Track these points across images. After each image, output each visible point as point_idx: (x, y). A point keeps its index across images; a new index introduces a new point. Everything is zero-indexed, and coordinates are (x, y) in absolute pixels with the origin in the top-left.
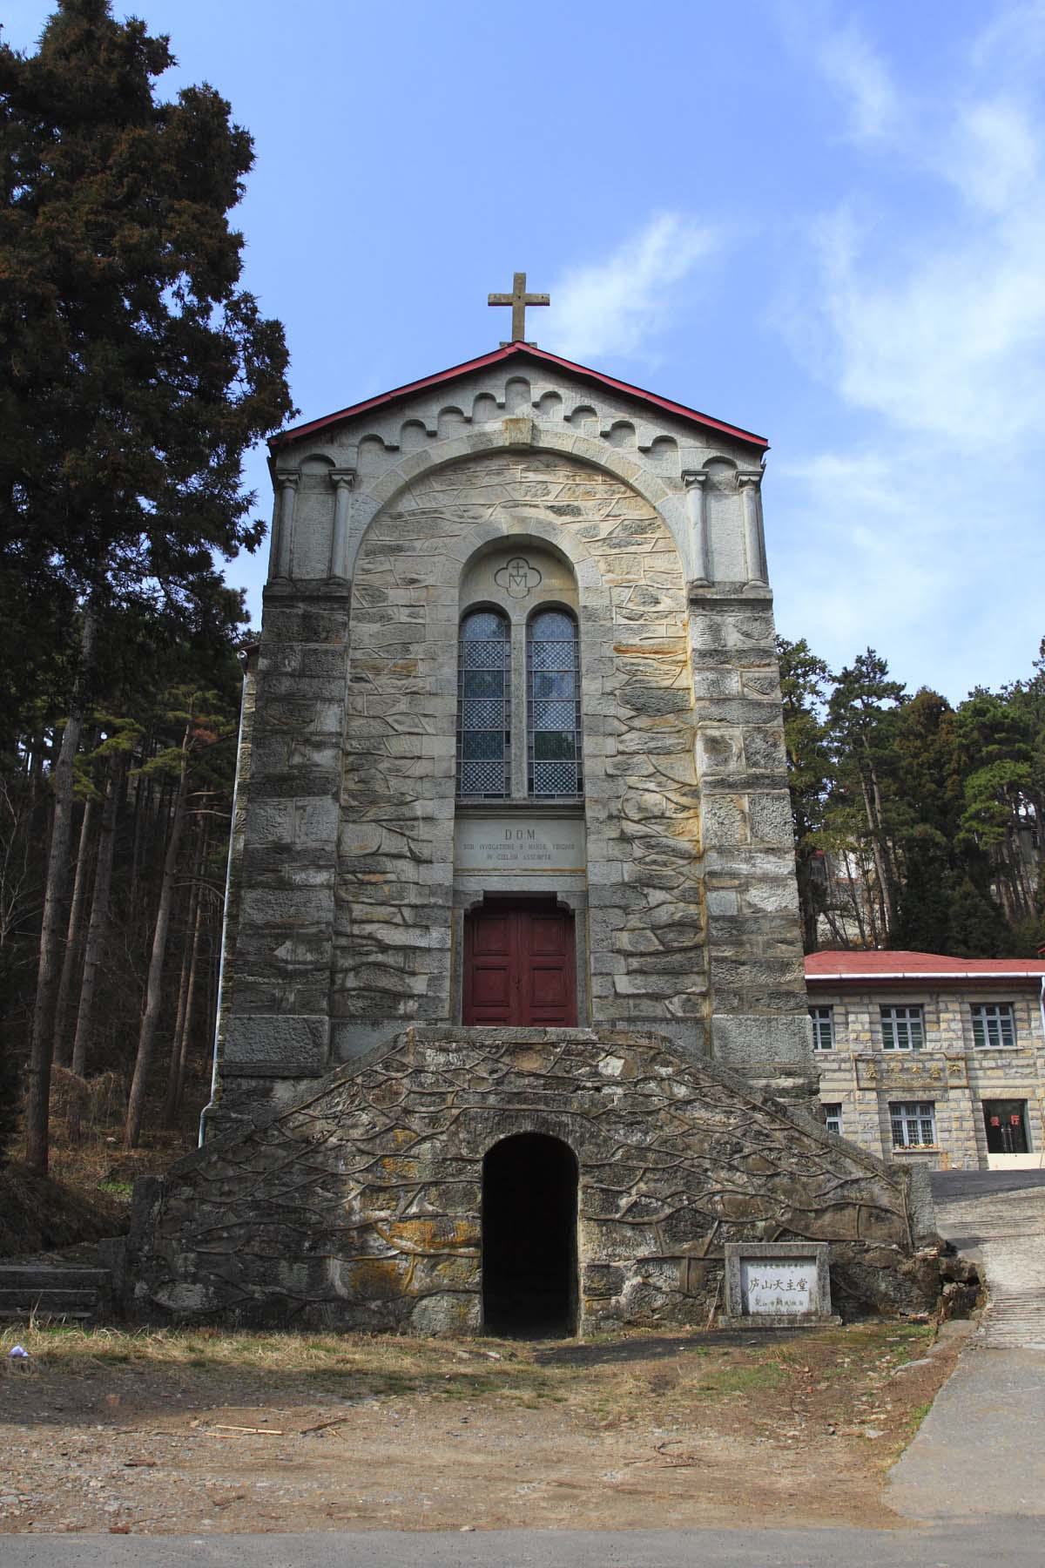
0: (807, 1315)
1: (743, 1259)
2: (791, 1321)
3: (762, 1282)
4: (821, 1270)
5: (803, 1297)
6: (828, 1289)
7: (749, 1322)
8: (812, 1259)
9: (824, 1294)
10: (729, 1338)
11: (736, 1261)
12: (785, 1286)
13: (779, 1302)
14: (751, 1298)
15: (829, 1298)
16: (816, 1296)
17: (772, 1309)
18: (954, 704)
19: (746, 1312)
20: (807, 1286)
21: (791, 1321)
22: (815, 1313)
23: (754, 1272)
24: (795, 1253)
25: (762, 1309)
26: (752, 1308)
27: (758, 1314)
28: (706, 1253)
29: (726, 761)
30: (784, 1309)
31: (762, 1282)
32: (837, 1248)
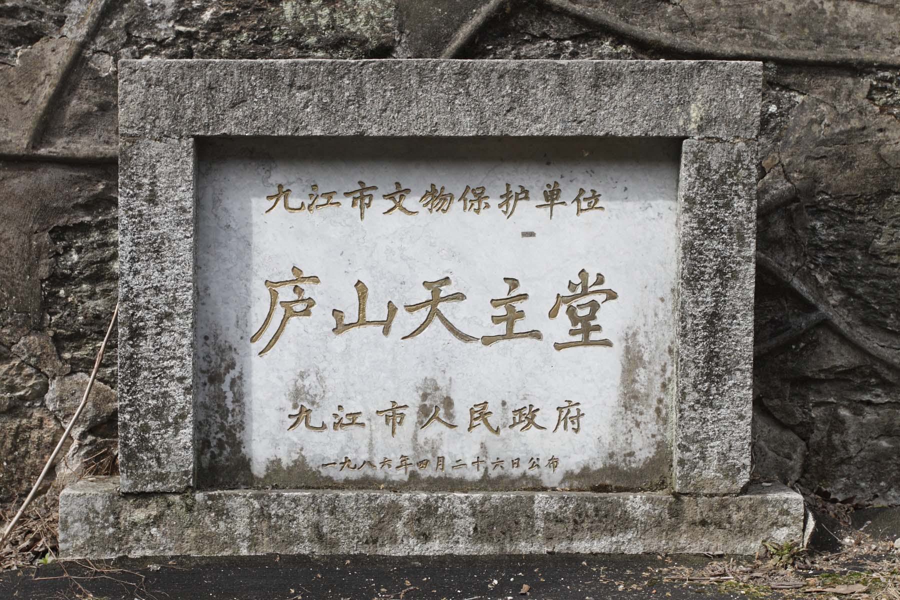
0: (603, 484)
1: (215, 154)
2: (490, 524)
3: (334, 292)
4: (705, 226)
5: (591, 379)
6: (742, 334)
7: (237, 527)
8: (656, 153)
9: (713, 370)
10: (215, 378)
11: (168, 167)
12: (473, 314)
13: (435, 407)
14: (266, 385)
15: (740, 388)
16: (659, 374)
17: (386, 448)
18: (259, 204)
19: (220, 464)
20: (611, 319)
21: (490, 524)
22: (652, 476)
23: (288, 233)
24: (546, 119)
25: (323, 448)
26: (267, 439)
27: (302, 476)
28: (45, 129)
29: (370, 500)
30: (460, 448)
31: (334, 292)
32: (815, 110)
